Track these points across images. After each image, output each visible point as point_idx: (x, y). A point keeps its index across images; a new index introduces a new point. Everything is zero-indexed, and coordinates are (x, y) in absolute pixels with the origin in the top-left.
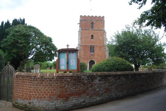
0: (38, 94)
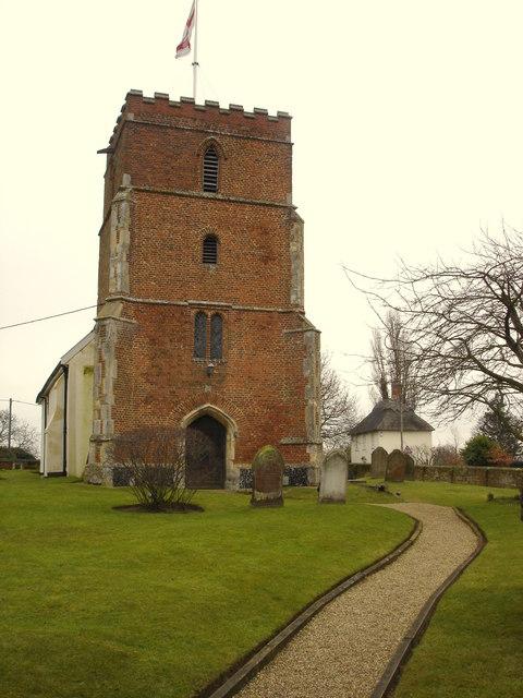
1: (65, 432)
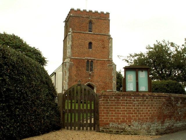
0: (139, 115)
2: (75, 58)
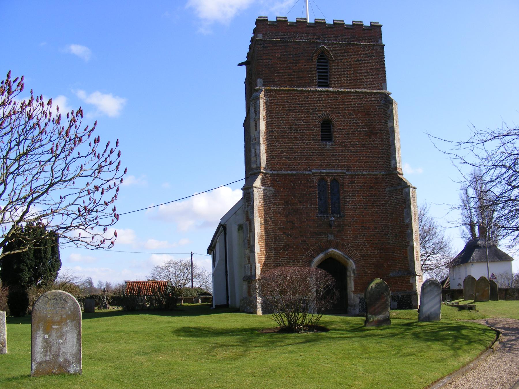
1: (227, 275)
2: (280, 172)
